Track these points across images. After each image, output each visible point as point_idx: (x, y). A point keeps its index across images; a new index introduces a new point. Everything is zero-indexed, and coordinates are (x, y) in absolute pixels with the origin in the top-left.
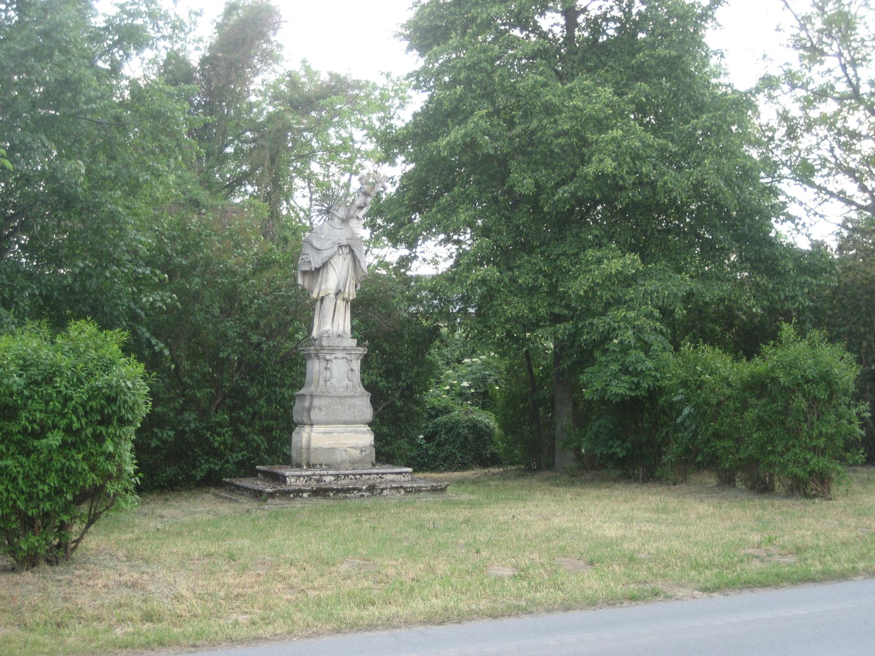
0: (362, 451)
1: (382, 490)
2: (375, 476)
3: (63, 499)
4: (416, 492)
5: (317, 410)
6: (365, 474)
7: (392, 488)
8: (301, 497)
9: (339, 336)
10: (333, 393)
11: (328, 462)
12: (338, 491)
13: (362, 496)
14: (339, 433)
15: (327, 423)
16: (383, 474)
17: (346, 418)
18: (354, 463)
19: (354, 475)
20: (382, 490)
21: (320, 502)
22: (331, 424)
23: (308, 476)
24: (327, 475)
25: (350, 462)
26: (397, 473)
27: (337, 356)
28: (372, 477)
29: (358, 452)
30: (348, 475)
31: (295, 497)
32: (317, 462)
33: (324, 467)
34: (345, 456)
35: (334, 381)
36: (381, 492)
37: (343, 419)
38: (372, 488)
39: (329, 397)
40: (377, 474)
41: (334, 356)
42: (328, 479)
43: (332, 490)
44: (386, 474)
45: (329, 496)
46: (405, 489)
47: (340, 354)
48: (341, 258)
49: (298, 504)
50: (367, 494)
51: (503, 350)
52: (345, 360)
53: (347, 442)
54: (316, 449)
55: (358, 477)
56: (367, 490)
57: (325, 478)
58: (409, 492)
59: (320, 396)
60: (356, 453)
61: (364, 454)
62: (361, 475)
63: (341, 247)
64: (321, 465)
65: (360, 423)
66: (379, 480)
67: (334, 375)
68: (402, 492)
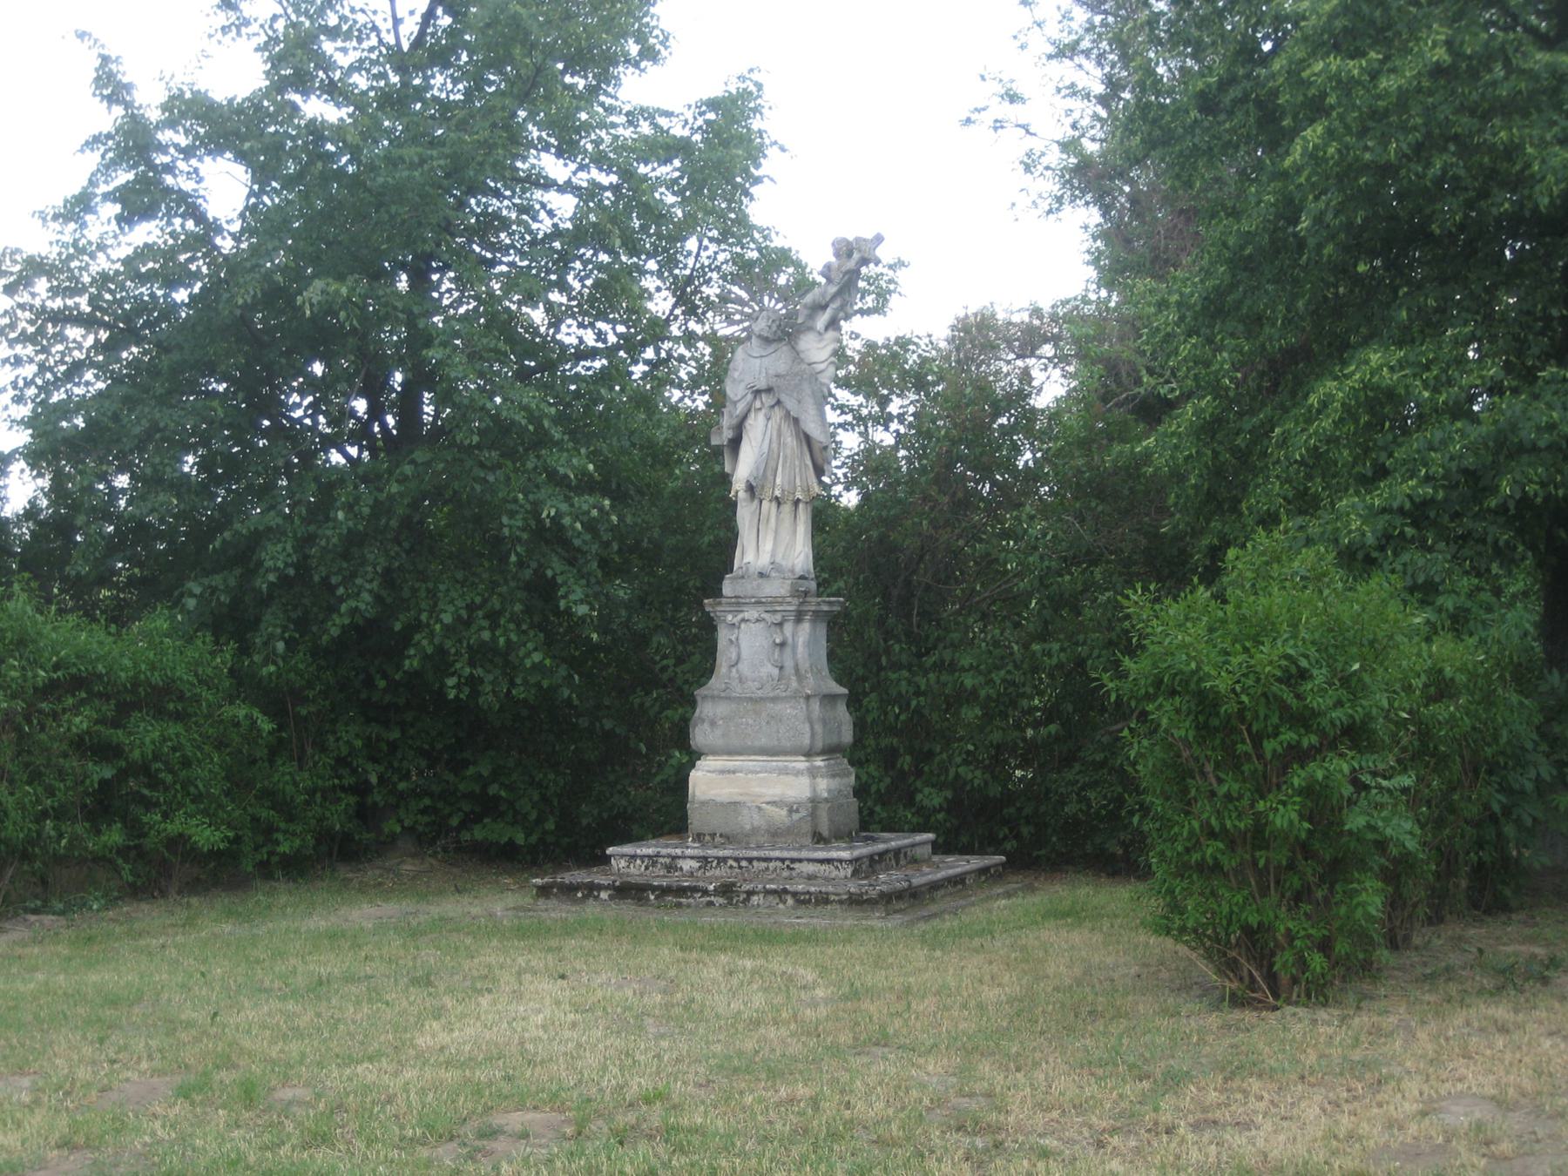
0: (791, 811)
1: (750, 893)
2: (779, 864)
3: (1376, 868)
4: (817, 903)
5: (706, 726)
6: (759, 859)
7: (768, 892)
8: (597, 898)
9: (761, 575)
10: (737, 690)
11: (726, 830)
12: (664, 891)
13: (710, 904)
14: (752, 772)
15: (730, 752)
16: (793, 860)
17: (763, 741)
18: (775, 834)
19: (737, 860)
20: (750, 893)
21: (627, 909)
22: (741, 754)
23: (649, 857)
24: (684, 857)
25: (768, 831)
26: (822, 861)
27: (746, 615)
28: (772, 865)
29: (784, 812)
30: (724, 860)
31: (585, 897)
32: (706, 830)
33: (718, 839)
34: (757, 820)
35: (744, 667)
36: (747, 899)
37: (757, 743)
38: (727, 890)
39: (728, 698)
40: (783, 860)
41: (740, 616)
42: (687, 865)
43: (654, 889)
44: (800, 861)
45: (648, 899)
46: (795, 894)
47: (751, 613)
48: (761, 416)
49: (591, 909)
50: (718, 900)
51: (470, 241)
52: (762, 625)
53: (764, 790)
54: (703, 803)
55: (744, 863)
56: (717, 892)
57: (681, 863)
58: (804, 902)
59: (713, 697)
60: (780, 814)
61: (796, 816)
62: (750, 860)
63: (757, 393)
64: (713, 835)
65: (794, 752)
66: (786, 874)
67: (745, 653)
68: (790, 901)
